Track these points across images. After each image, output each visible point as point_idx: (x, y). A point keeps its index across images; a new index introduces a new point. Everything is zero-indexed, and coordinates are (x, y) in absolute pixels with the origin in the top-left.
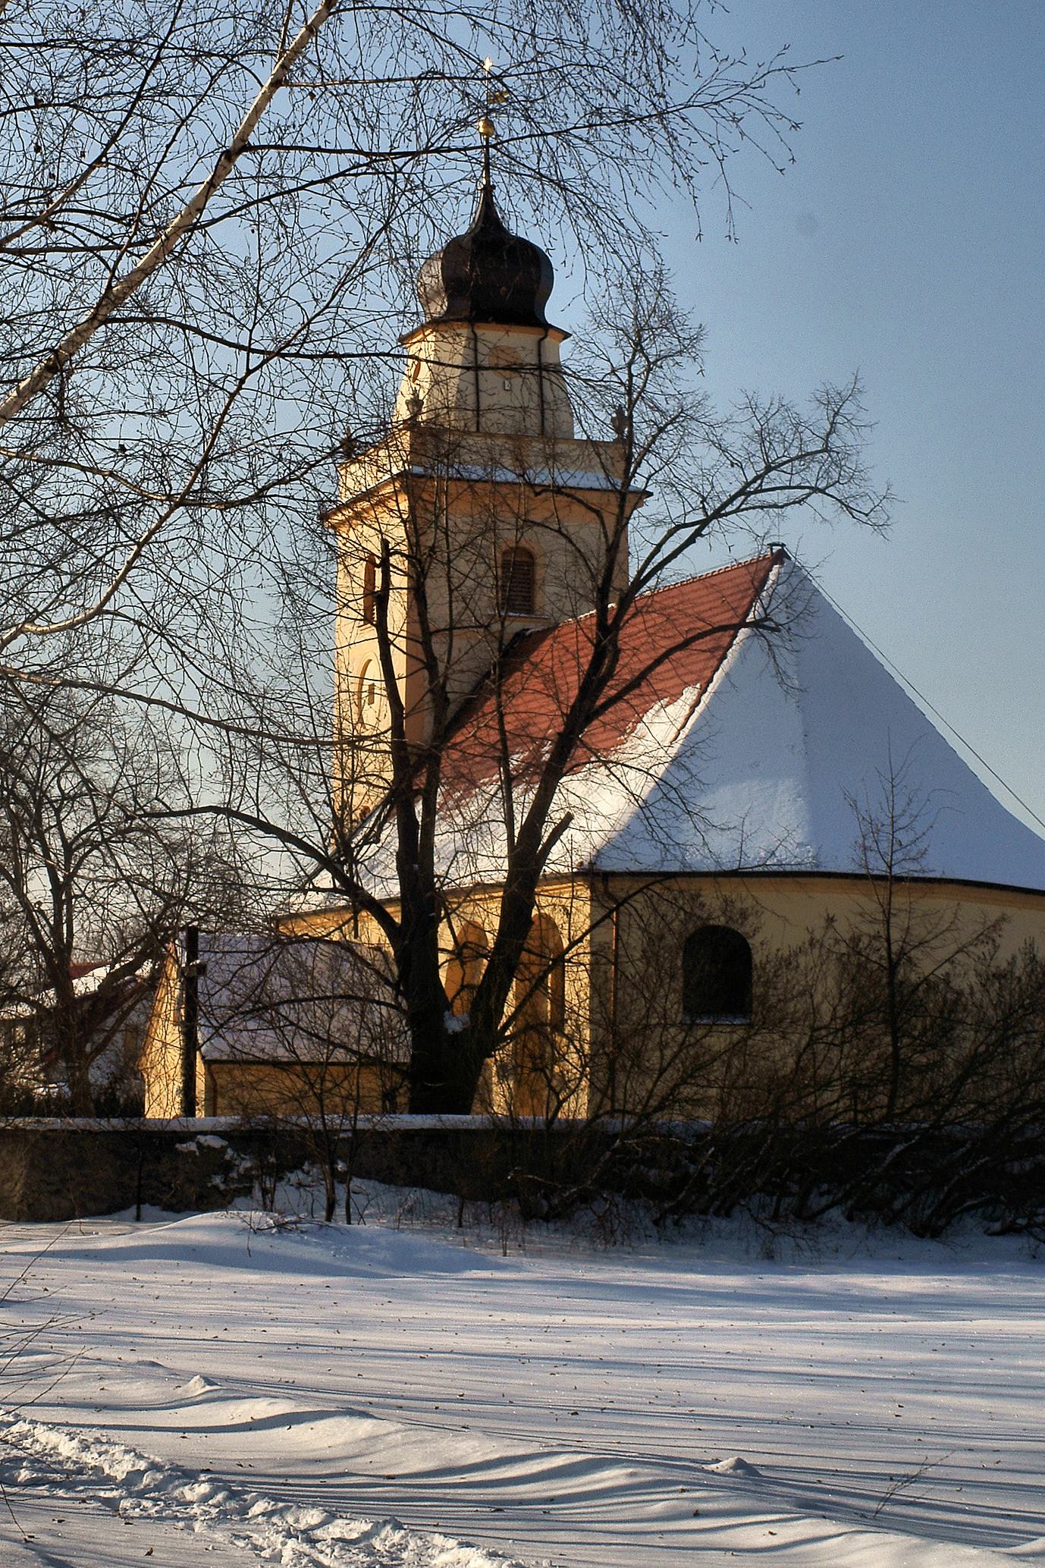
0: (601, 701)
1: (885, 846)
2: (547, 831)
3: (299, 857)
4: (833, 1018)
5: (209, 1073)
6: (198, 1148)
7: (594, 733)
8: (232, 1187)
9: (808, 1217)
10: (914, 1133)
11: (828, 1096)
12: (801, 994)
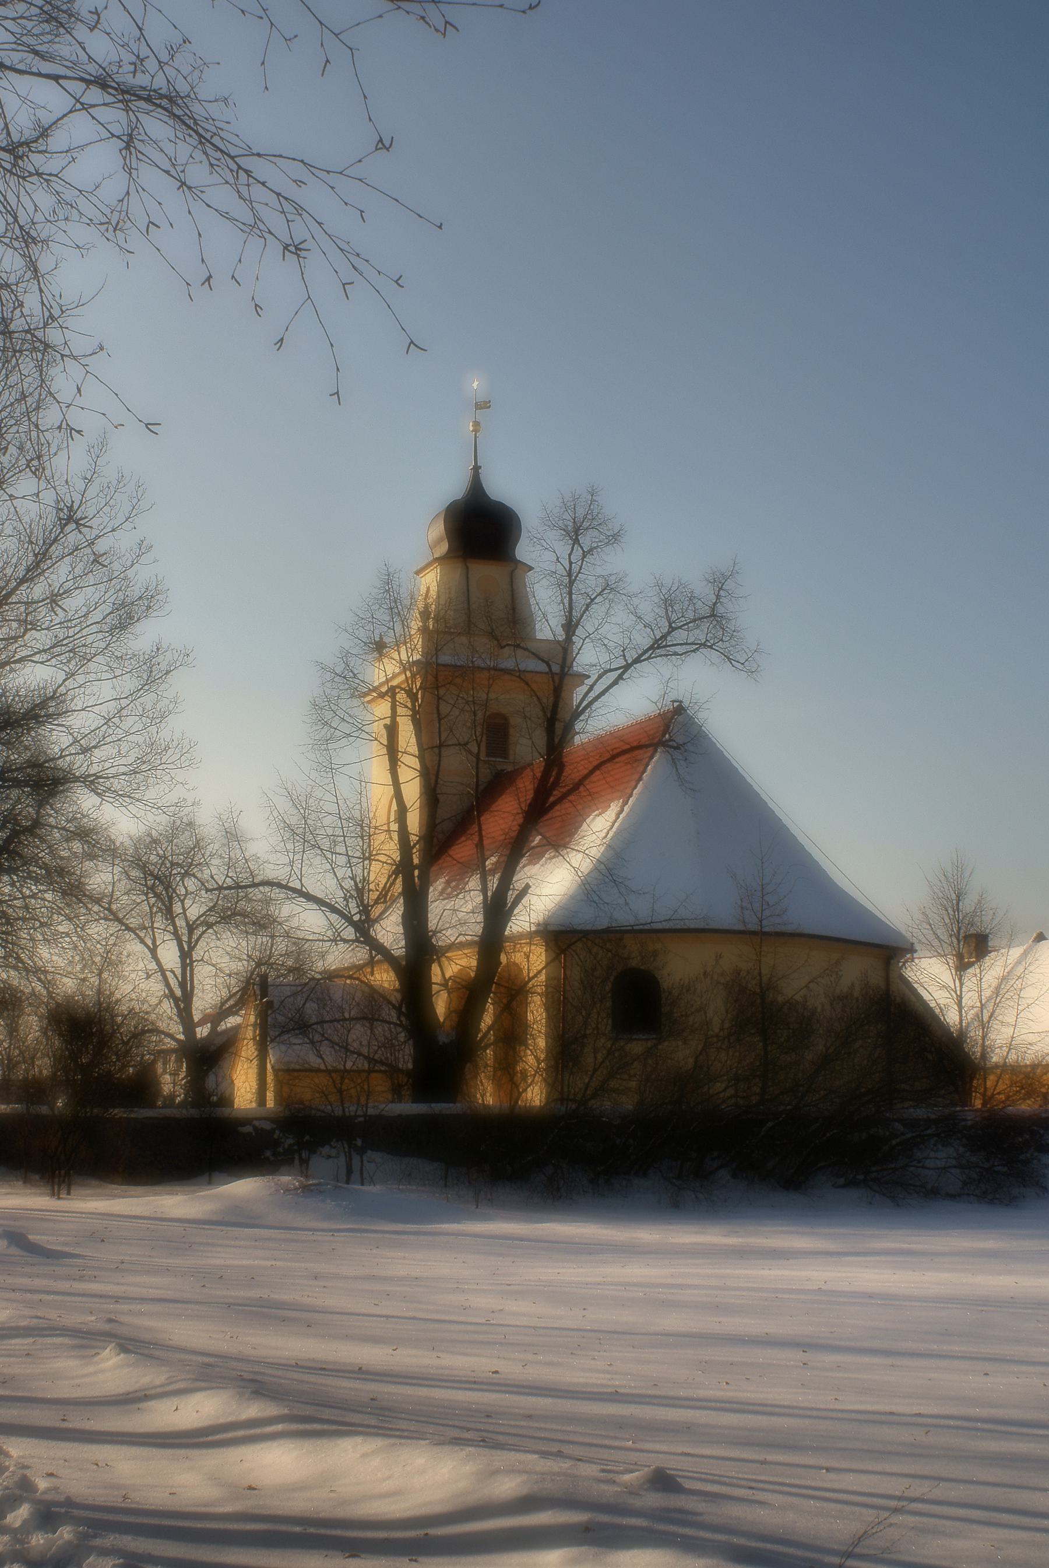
3: (327, 913)
4: (722, 1029)
11: (719, 1086)
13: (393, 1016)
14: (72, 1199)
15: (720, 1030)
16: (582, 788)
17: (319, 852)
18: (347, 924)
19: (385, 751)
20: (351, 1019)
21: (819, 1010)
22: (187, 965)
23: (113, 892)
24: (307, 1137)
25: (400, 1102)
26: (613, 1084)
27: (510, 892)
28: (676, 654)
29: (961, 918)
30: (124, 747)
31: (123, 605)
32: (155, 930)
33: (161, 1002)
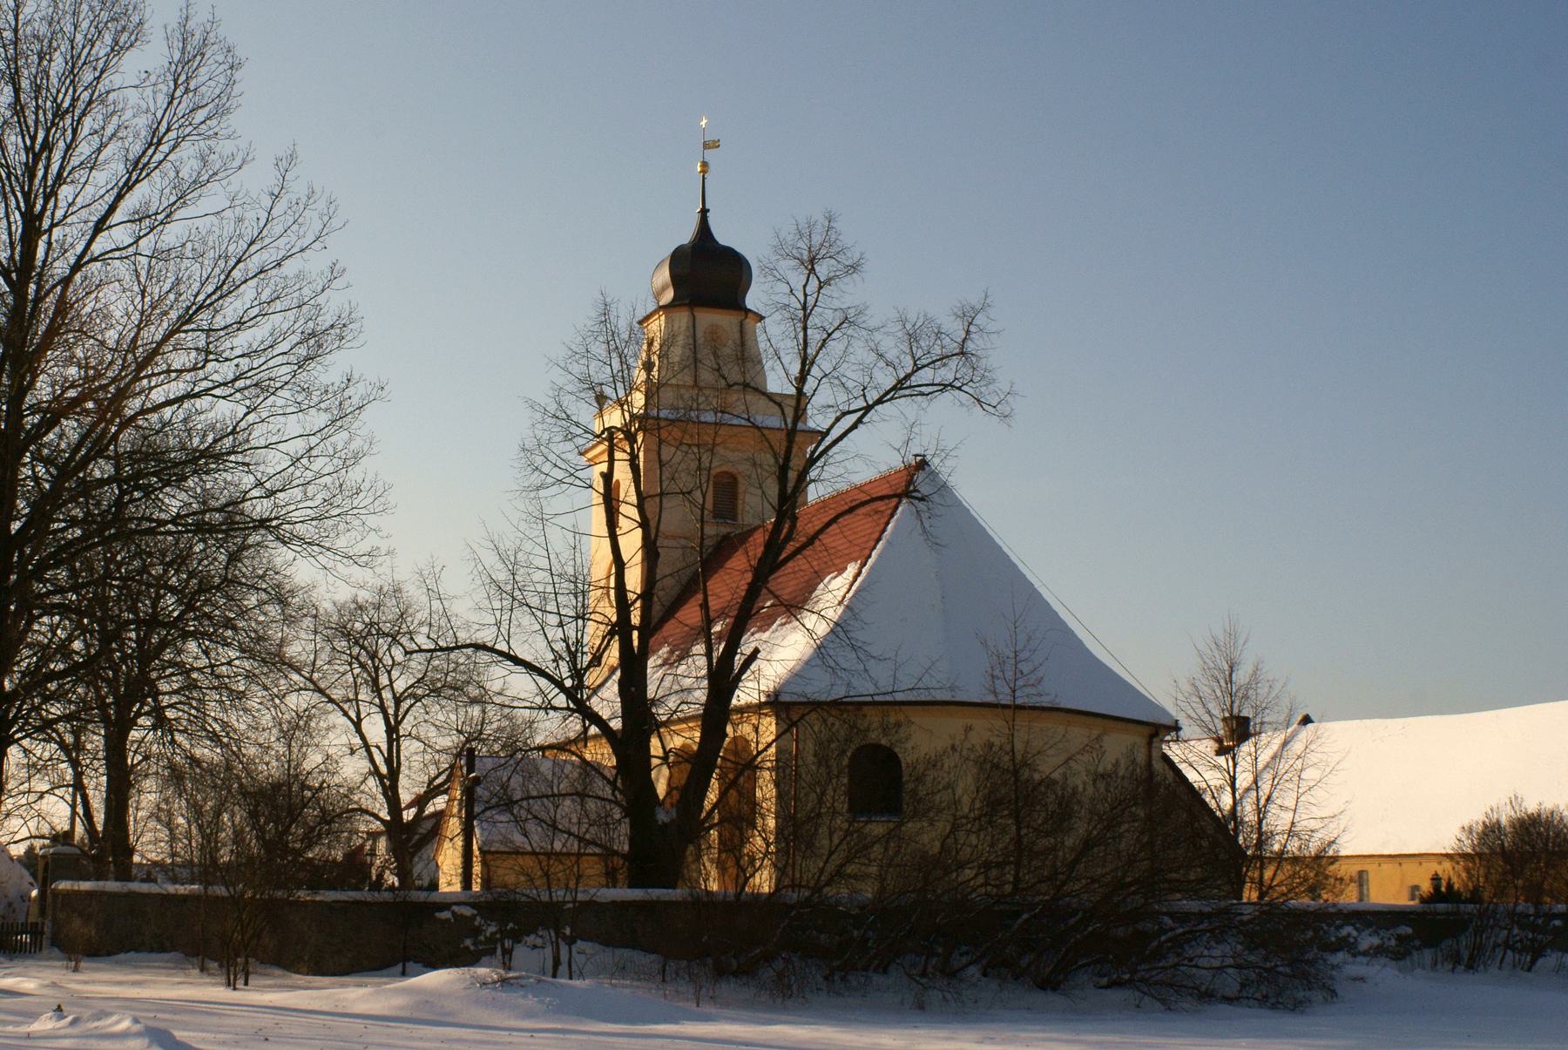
1: (1009, 675)
2: (738, 660)
5: (484, 863)
7: (785, 581)
9: (951, 974)
10: (1038, 904)
11: (968, 873)
12: (945, 788)
13: (607, 792)
14: (249, 990)
15: (970, 811)
16: (817, 543)
18: (557, 690)
19: (601, 500)
21: (1081, 788)
22: (394, 740)
23: (315, 661)
24: (511, 925)
25: (615, 887)
26: (850, 869)
27: (737, 657)
28: (922, 394)
29: (1234, 690)
30: (311, 489)
31: (313, 334)
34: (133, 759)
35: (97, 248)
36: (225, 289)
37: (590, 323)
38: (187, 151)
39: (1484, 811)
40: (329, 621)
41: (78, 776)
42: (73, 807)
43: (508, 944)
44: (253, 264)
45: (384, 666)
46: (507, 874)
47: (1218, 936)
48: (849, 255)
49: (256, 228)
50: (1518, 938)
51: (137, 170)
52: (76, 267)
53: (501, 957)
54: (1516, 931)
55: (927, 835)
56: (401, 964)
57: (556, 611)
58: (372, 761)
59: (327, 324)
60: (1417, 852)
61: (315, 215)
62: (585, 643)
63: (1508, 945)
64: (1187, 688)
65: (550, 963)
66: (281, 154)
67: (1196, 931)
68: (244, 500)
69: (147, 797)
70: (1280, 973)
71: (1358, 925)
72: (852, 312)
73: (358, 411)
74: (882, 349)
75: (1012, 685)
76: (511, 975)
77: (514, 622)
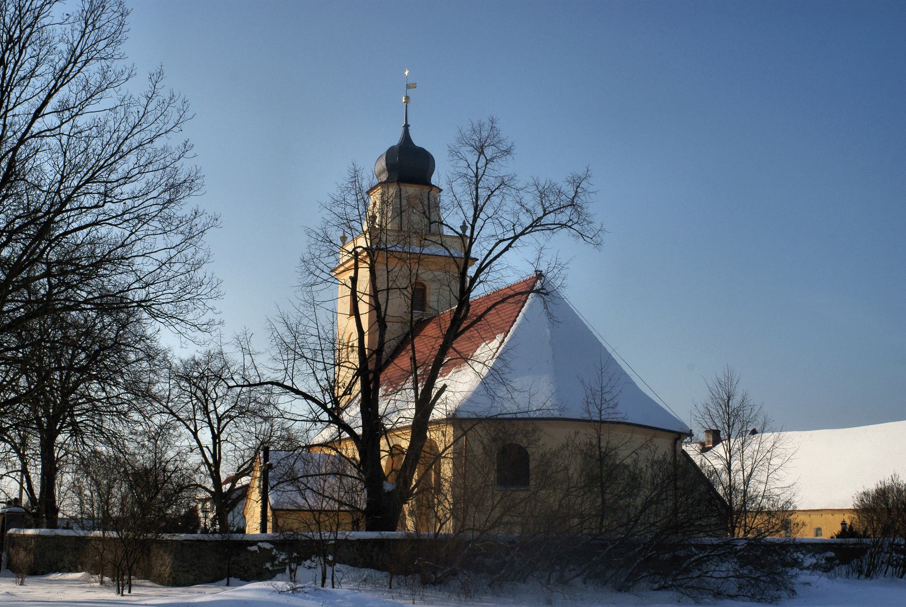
0: (461, 328)
1: (598, 401)
2: (434, 392)
5: (274, 514)
6: (259, 549)
7: (460, 344)
8: (276, 568)
9: (563, 582)
13: (354, 472)
17: (304, 359)
18: (322, 410)
20: (326, 474)
21: (644, 470)
23: (169, 395)
25: (358, 531)
26: (506, 519)
28: (549, 229)
30: (171, 283)
31: (173, 186)
32: (197, 421)
33: (199, 466)
34: (58, 453)
35: (35, 129)
36: (119, 154)
37: (345, 183)
38: (94, 67)
39: (876, 483)
40: (178, 372)
41: (24, 465)
42: (21, 484)
43: (293, 566)
44: (134, 141)
45: (211, 399)
46: (293, 522)
47: (723, 558)
48: (504, 143)
49: (137, 117)
50: (894, 558)
51: (62, 77)
52: (22, 141)
53: (289, 574)
54: (894, 554)
55: (552, 498)
56: (226, 579)
57: (322, 361)
58: (204, 456)
59: (182, 180)
60: (820, 509)
61: (175, 110)
62: (339, 381)
63: (889, 563)
64: (702, 409)
65: (320, 577)
66: (153, 71)
67: (711, 556)
68: (128, 290)
69: (66, 478)
70: (761, 581)
71: (804, 552)
72: (506, 179)
73: (201, 234)
74: (524, 202)
75: (599, 407)
76: (298, 586)
77: (296, 368)
